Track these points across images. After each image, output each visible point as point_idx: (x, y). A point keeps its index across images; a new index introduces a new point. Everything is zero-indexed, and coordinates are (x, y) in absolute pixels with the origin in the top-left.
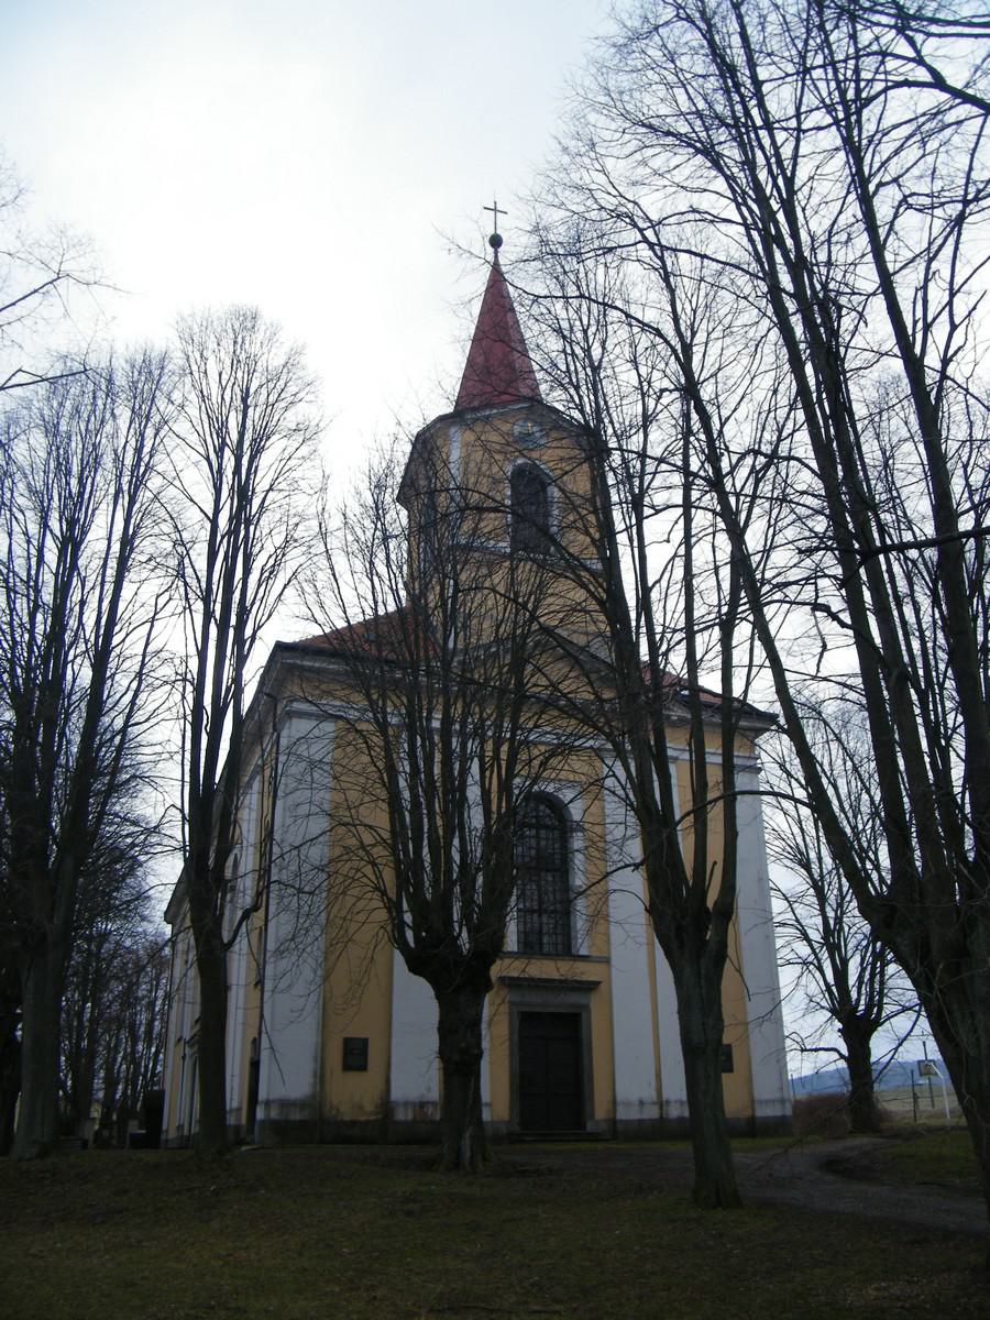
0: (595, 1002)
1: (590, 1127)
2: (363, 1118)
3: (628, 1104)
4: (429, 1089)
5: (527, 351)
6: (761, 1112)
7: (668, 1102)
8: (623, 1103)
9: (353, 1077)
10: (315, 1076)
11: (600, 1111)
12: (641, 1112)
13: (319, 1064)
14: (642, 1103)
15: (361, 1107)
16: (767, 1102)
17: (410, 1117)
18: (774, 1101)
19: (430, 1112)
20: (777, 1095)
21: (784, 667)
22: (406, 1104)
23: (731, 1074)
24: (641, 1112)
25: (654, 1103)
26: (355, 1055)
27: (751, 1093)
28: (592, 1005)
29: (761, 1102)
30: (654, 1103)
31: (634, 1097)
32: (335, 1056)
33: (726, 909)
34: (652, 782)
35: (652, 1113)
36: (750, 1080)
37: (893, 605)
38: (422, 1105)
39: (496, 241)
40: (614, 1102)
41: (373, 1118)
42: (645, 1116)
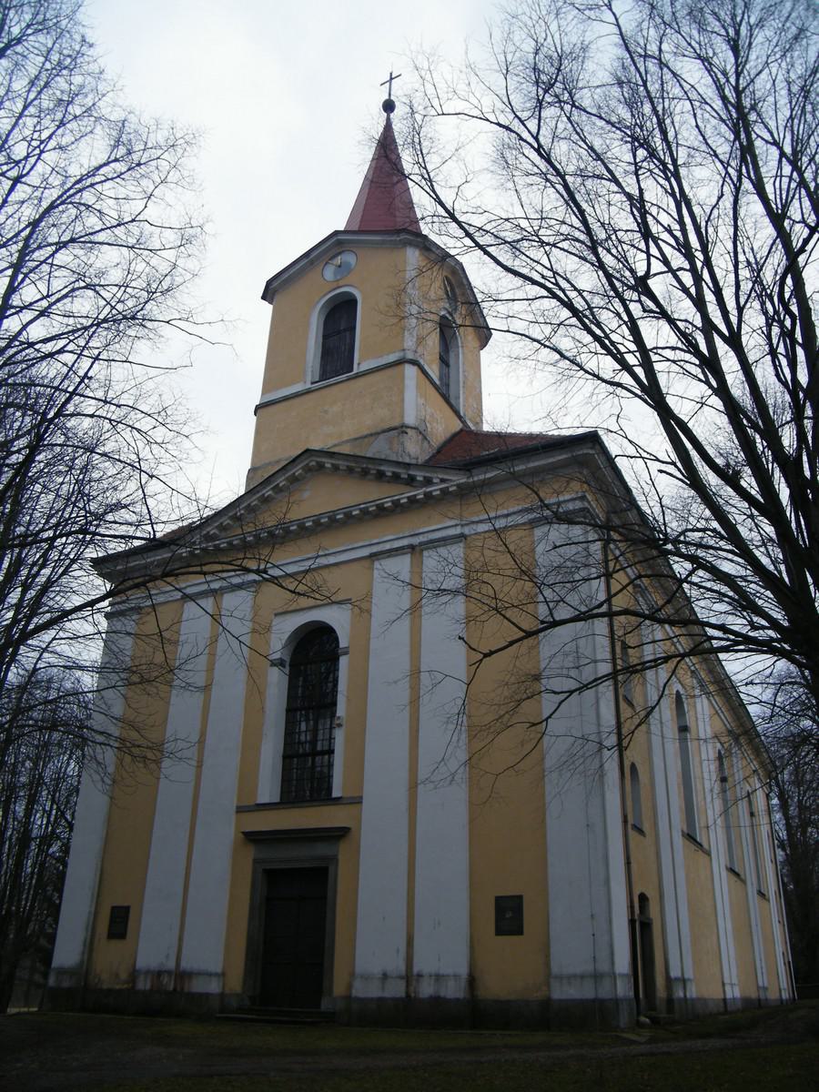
0: (343, 850)
1: (325, 1004)
2: (118, 987)
3: (367, 978)
4: (167, 956)
5: (416, 221)
6: (560, 992)
7: (420, 975)
8: (362, 977)
9: (116, 944)
10: (84, 945)
11: (339, 989)
12: (383, 989)
13: (89, 933)
14: (385, 976)
15: (117, 975)
16: (571, 978)
17: (148, 987)
18: (582, 977)
19: (165, 982)
20: (589, 968)
21: (690, 274)
22: (148, 972)
23: (521, 937)
24: (383, 989)
25: (401, 977)
26: (509, 915)
27: (547, 964)
28: (340, 857)
29: (560, 978)
30: (401, 977)
31: (376, 969)
32: (103, 927)
33: (412, 486)
34: (436, 524)
35: (396, 990)
36: (546, 946)
37: (792, 567)
38: (159, 973)
39: (389, 106)
40: (352, 974)
41: (126, 986)
42: (387, 994)
